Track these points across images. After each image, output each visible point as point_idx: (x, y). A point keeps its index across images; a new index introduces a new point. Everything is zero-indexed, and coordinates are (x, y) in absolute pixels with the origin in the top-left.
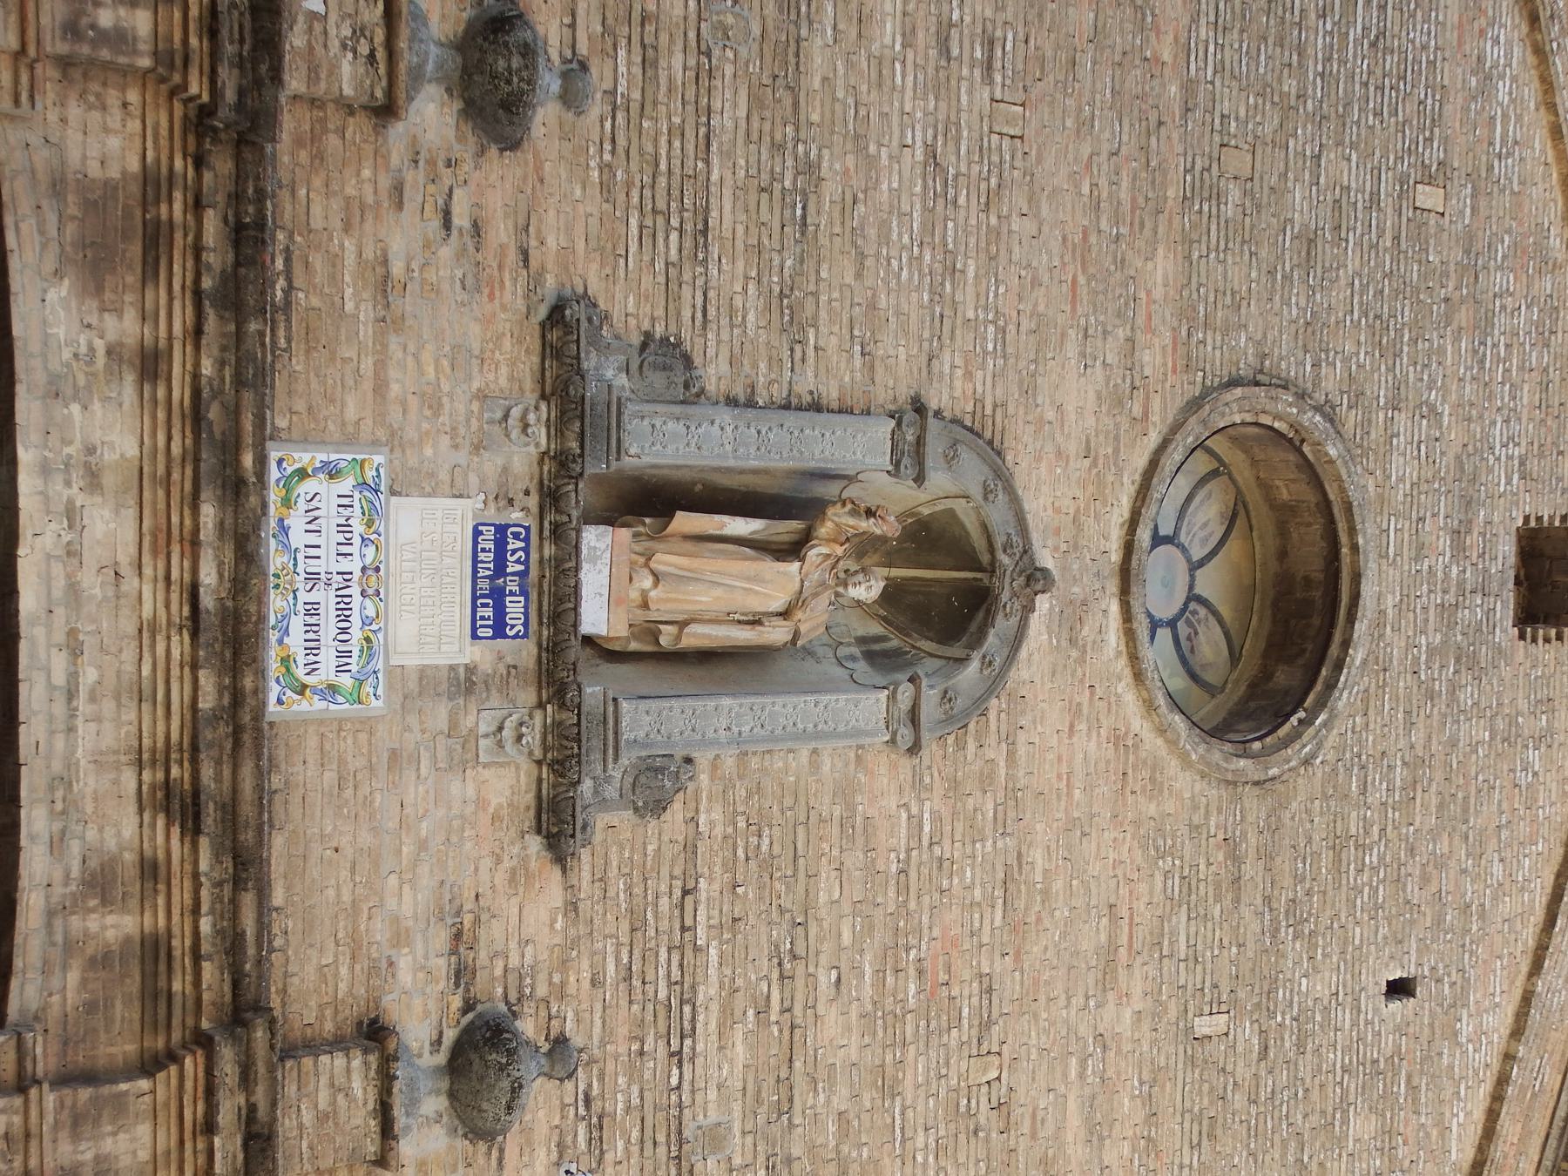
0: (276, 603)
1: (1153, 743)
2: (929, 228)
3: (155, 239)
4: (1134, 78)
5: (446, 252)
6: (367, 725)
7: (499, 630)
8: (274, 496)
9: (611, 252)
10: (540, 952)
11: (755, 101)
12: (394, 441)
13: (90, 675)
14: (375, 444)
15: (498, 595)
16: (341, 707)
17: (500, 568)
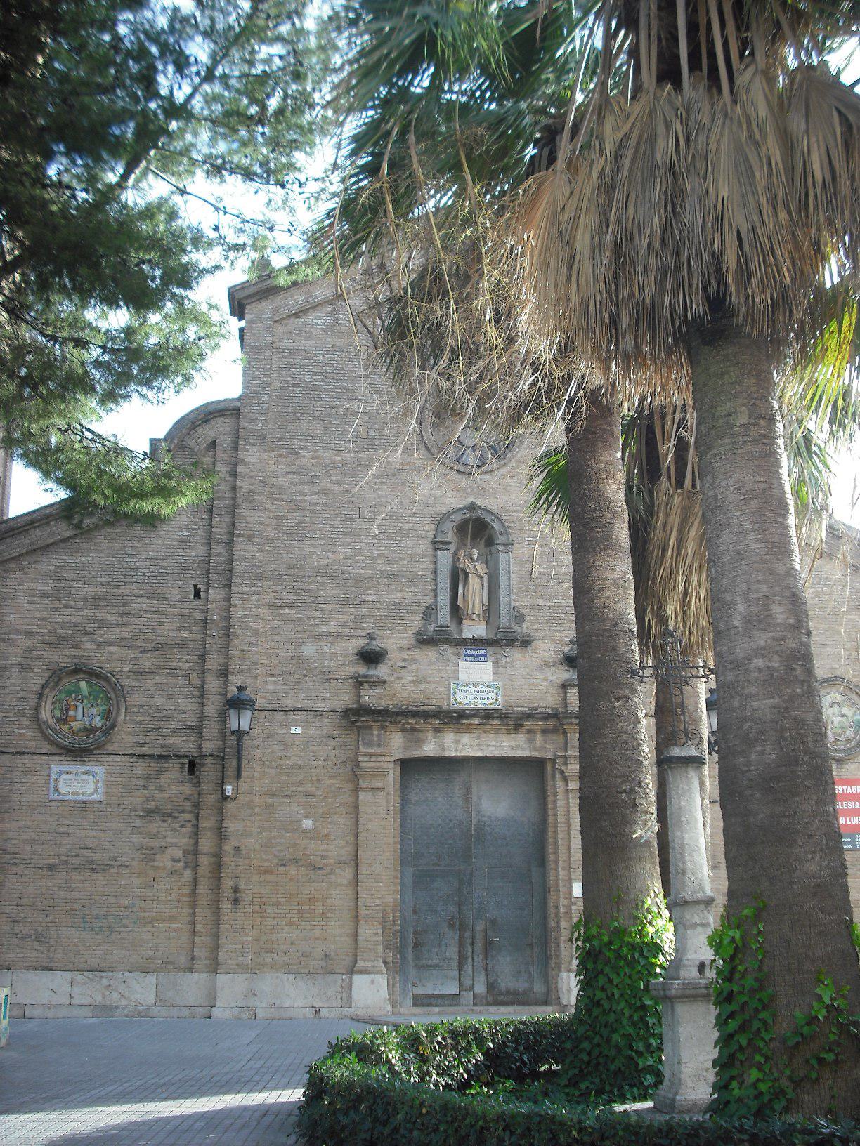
0: (480, 706)
1: (513, 463)
2: (392, 538)
3: (413, 730)
4: (348, 469)
5: (409, 668)
6: (504, 686)
7: (485, 656)
8: (460, 706)
9: (406, 627)
10: (551, 646)
11: (369, 589)
12: (448, 680)
13: (493, 742)
14: (449, 684)
15: (478, 656)
16: (500, 693)
17: (472, 655)
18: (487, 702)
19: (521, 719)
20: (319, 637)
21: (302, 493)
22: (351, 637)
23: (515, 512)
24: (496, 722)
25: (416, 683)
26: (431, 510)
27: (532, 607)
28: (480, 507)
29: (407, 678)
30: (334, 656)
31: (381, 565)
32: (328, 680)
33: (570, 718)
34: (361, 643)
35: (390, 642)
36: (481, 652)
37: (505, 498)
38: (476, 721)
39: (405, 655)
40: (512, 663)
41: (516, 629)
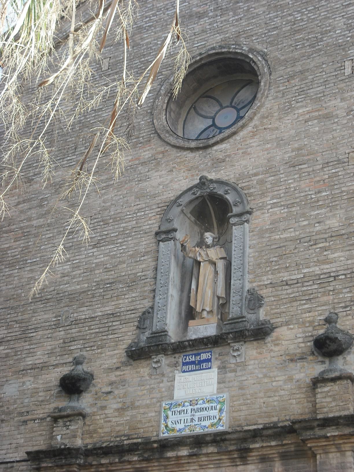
1: (256, 121)
7: (208, 360)
8: (172, 434)
9: (117, 342)
14: (161, 406)
15: (200, 362)
16: (225, 408)
17: (193, 363)
18: (207, 423)
19: (244, 440)
20: (23, 372)
21: (29, 219)
22: (56, 366)
23: (256, 175)
24: (211, 449)
25: (122, 410)
26: (158, 200)
27: (272, 285)
28: (211, 181)
29: (113, 405)
30: (36, 391)
31: (99, 275)
32: (25, 422)
33: (312, 428)
34: (66, 370)
35: (98, 363)
36: (204, 356)
37: (244, 163)
38: (184, 452)
39: (113, 377)
40: (244, 365)
41: (251, 317)
